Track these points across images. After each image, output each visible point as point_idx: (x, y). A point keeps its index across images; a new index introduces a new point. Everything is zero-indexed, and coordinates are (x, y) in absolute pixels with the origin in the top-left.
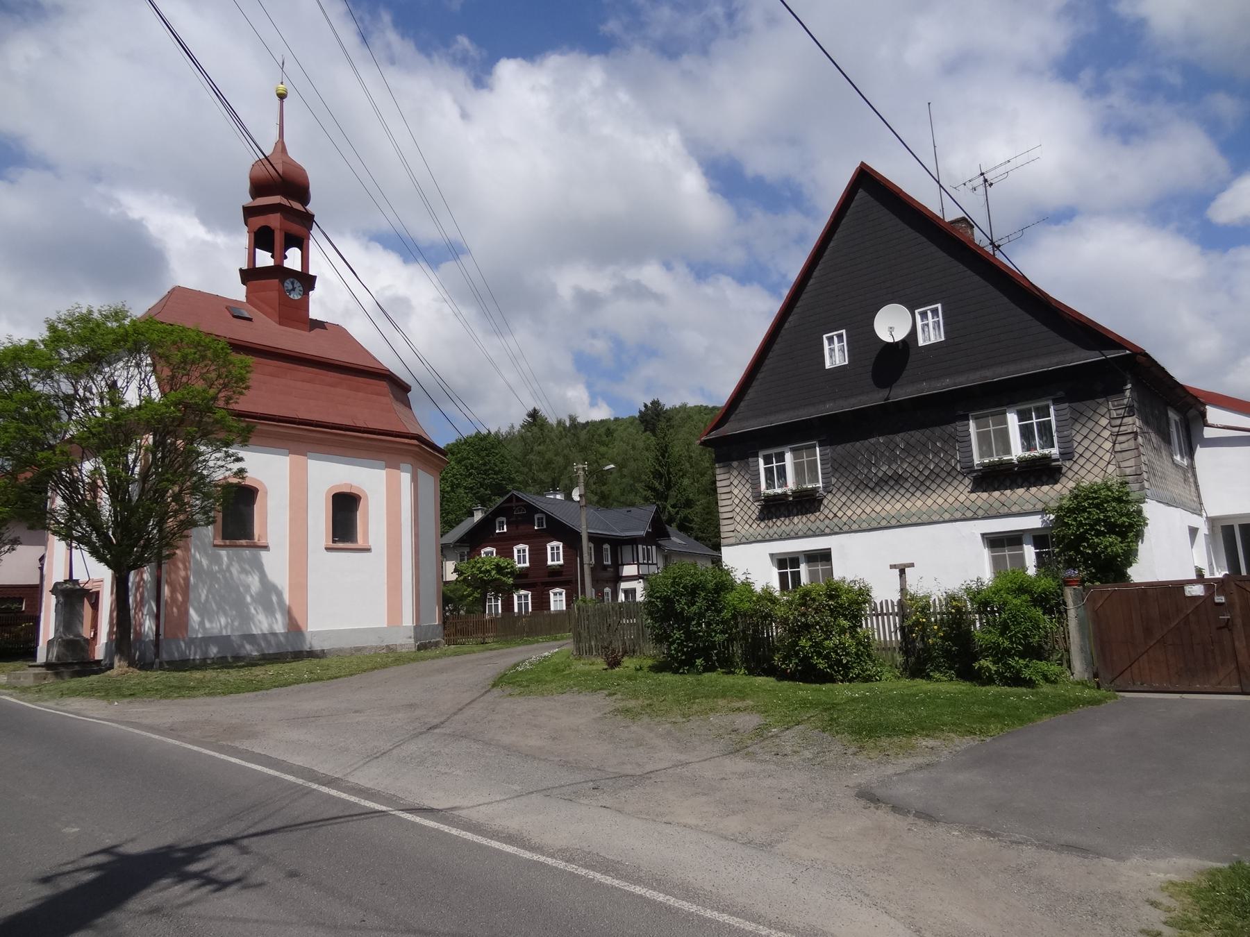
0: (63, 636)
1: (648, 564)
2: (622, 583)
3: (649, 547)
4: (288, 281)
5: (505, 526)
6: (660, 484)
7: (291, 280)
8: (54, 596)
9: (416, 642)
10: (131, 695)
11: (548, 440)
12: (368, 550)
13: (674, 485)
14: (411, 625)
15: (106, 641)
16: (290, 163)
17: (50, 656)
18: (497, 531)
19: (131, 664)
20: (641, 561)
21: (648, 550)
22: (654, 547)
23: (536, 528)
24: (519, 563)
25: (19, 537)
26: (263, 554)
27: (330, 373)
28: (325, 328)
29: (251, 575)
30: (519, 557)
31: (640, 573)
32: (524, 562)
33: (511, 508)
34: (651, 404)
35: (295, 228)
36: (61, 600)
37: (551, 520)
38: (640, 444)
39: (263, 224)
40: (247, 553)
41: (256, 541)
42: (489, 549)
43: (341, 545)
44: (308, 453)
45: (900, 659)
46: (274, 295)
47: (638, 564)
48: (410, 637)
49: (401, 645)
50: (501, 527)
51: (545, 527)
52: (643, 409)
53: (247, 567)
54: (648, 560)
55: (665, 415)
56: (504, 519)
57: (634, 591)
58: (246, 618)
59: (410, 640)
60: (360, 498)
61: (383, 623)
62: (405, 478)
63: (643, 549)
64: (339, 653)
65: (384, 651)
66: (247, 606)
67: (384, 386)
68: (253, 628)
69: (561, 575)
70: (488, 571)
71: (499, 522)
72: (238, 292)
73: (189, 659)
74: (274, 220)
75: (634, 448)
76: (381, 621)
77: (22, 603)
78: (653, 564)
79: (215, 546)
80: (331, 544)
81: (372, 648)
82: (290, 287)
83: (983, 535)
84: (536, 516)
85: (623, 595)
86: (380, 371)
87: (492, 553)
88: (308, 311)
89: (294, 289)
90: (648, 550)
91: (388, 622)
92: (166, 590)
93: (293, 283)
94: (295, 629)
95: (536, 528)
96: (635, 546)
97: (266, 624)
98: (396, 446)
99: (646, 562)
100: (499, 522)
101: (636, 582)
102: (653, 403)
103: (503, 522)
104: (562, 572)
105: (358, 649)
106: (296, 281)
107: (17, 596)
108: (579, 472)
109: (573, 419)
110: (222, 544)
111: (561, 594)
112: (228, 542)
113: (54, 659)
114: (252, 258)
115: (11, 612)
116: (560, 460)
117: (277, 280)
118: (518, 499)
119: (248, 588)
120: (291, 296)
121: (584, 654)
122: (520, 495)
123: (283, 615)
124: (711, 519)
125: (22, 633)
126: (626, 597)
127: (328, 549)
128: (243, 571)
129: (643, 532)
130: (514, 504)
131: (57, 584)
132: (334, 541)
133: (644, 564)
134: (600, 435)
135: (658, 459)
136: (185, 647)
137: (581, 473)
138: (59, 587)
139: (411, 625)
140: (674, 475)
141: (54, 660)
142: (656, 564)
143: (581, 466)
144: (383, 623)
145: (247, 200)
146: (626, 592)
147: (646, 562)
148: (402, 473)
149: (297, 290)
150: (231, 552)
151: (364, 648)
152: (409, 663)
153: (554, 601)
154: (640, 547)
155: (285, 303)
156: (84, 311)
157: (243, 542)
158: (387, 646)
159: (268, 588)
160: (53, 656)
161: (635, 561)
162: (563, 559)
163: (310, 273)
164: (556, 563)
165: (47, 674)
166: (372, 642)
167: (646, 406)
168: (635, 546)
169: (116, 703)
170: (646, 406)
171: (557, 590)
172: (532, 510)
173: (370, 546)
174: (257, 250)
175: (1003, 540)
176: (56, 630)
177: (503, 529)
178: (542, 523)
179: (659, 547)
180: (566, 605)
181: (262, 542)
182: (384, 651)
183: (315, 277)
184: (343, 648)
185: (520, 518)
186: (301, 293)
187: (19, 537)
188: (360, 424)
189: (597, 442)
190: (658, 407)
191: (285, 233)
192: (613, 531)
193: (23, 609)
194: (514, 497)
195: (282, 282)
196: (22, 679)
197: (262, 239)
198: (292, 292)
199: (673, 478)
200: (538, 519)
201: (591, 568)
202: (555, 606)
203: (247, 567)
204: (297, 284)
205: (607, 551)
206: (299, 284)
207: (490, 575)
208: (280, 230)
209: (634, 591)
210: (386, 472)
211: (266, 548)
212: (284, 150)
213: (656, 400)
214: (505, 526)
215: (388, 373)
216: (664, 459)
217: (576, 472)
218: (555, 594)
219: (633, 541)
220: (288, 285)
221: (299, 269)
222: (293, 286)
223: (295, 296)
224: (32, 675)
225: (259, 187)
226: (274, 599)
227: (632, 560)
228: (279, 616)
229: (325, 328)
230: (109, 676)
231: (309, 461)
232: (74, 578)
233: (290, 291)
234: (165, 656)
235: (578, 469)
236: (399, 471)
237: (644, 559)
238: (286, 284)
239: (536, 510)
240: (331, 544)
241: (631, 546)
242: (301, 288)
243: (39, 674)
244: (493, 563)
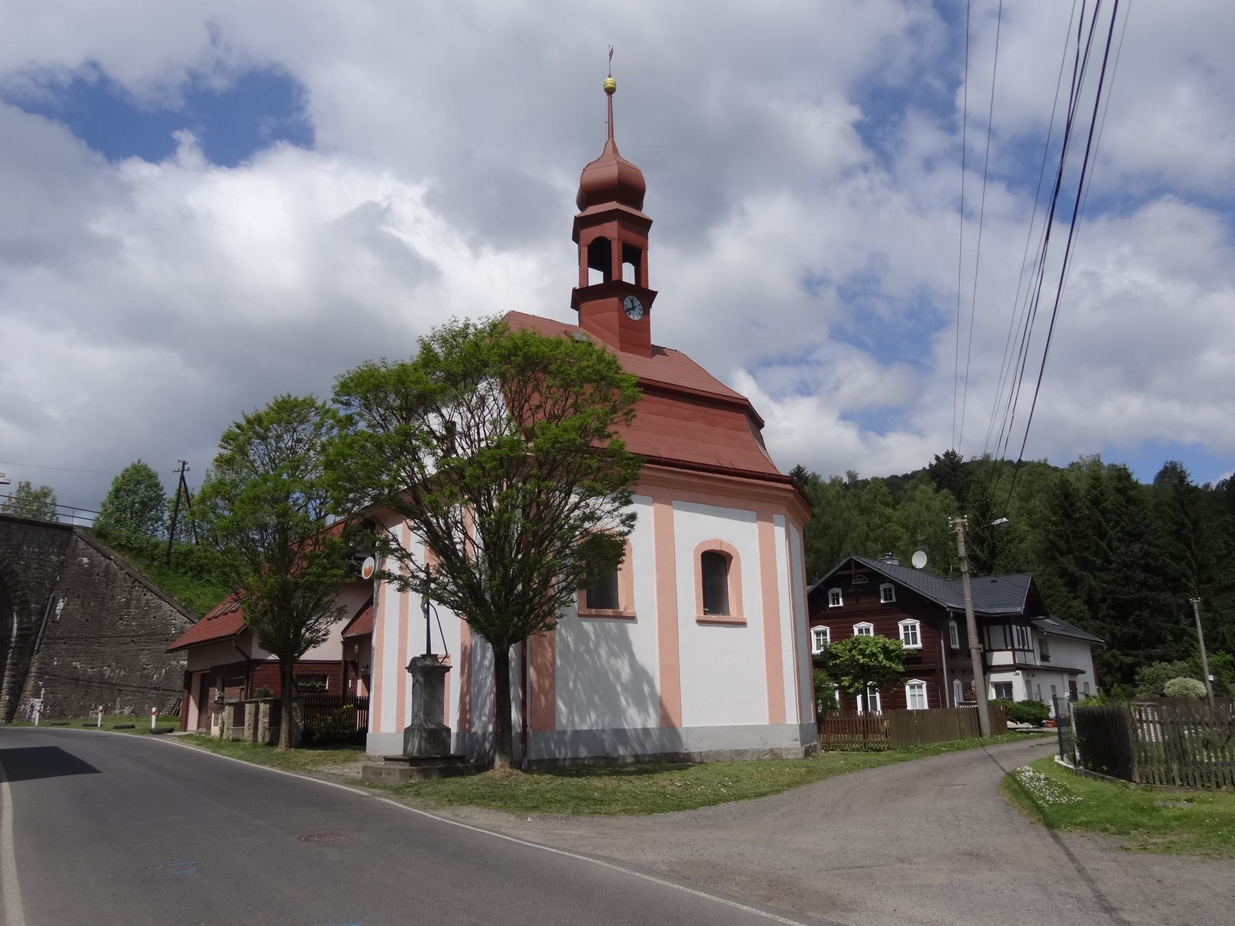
0: (424, 724)
1: (1024, 650)
2: (992, 675)
3: (1024, 628)
4: (627, 299)
5: (841, 600)
6: (982, 551)
7: (631, 297)
8: (411, 675)
9: (802, 744)
10: (534, 807)
11: (823, 501)
12: (743, 624)
13: (1001, 552)
14: (796, 723)
15: (456, 732)
16: (622, 165)
17: (410, 747)
18: (831, 606)
19: (516, 765)
20: (1016, 646)
21: (1022, 631)
22: (1029, 628)
23: (882, 601)
24: (908, 643)
25: (345, 606)
26: (630, 626)
27: (684, 404)
28: (664, 354)
29: (620, 657)
30: (906, 635)
31: (1017, 662)
32: (915, 642)
33: (850, 577)
34: (944, 455)
35: (632, 237)
36: (421, 679)
37: (902, 590)
38: (937, 505)
39: (598, 235)
40: (612, 625)
41: (622, 609)
42: (863, 625)
43: (714, 617)
44: (673, 501)
45: (595, 728)
46: (613, 317)
47: (1013, 650)
48: (796, 740)
49: (787, 749)
50: (836, 600)
51: (894, 600)
52: (934, 462)
53: (616, 648)
54: (1024, 645)
55: (961, 469)
56: (839, 591)
57: (1008, 686)
58: (618, 713)
59: (795, 743)
60: (730, 557)
61: (764, 720)
62: (779, 532)
63: (1017, 630)
64: (717, 756)
65: (767, 756)
66: (617, 695)
67: (742, 418)
68: (624, 723)
69: (920, 663)
70: (873, 655)
71: (833, 595)
72: (571, 318)
73: (558, 759)
74: (611, 230)
75: (928, 508)
76: (760, 717)
77: (326, 682)
78: (1029, 651)
79: (580, 616)
80: (702, 616)
81: (754, 752)
82: (630, 306)
83: (637, 623)
84: (882, 587)
85: (994, 690)
86: (737, 401)
87: (868, 631)
88: (649, 333)
89: (633, 308)
90: (1022, 631)
91: (771, 718)
92: (532, 673)
93: (632, 302)
94: (668, 724)
95: (882, 601)
96: (1007, 627)
97: (638, 719)
98: (761, 491)
99: (1021, 647)
100: (833, 595)
101: (1012, 673)
102: (947, 455)
103: (838, 594)
104: (921, 658)
105: (740, 753)
106: (635, 299)
107: (321, 673)
108: (957, 528)
109: (852, 476)
110: (588, 613)
111: (920, 687)
112: (593, 611)
113: (415, 751)
114: (584, 276)
115: (314, 692)
116: (839, 523)
117: (616, 298)
118: (859, 565)
119: (617, 675)
120: (631, 317)
121: (1157, 782)
122: (863, 560)
123: (655, 709)
124: (1054, 595)
125: (344, 716)
126: (998, 693)
127: (700, 622)
128: (612, 653)
129: (1020, 608)
130: (853, 571)
131: (414, 660)
132: (705, 613)
133: (1019, 650)
134: (884, 495)
135: (978, 520)
136: (555, 748)
137: (959, 529)
138: (419, 664)
139: (796, 723)
140: (1000, 539)
141: (415, 753)
142: (1033, 651)
143: (958, 520)
144: (764, 720)
145: (577, 212)
146: (998, 686)
147: (1021, 647)
148: (775, 527)
149: (637, 309)
150: (596, 624)
151: (746, 751)
152: (838, 774)
153: (911, 696)
154: (1014, 627)
155: (625, 323)
156: (461, 325)
157: (609, 612)
158: (771, 750)
159: (639, 673)
160: (413, 749)
161: (1008, 646)
162: (922, 642)
163: (650, 289)
164: (911, 646)
165: (412, 770)
166: (752, 743)
167: (937, 458)
168: (1007, 627)
169: (529, 820)
170: (937, 458)
171: (915, 681)
172: (877, 578)
173: (745, 619)
174: (589, 268)
175: (908, 627)
176: (414, 716)
177: (838, 603)
178: (891, 595)
179: (1035, 628)
180: (929, 702)
181: (628, 613)
182: (767, 756)
183: (655, 293)
184: (722, 751)
185: (860, 590)
186: (642, 312)
187: (345, 606)
188: (726, 464)
189: (882, 503)
190: (954, 459)
191: (623, 243)
192: (982, 608)
193: (327, 688)
194: (852, 561)
195: (622, 301)
196: (383, 776)
197: (597, 255)
198: (632, 311)
199: (997, 543)
200: (885, 590)
201: (981, 653)
202: (913, 703)
203: (616, 648)
204: (637, 303)
205: (954, 631)
206: (638, 302)
207: (877, 659)
208: (618, 240)
209: (1008, 686)
210: (758, 525)
211: (632, 619)
212: (615, 150)
213: (950, 451)
214: (841, 600)
215: (746, 403)
216: (984, 519)
217: (953, 529)
218: (912, 687)
219: (1005, 620)
220: (628, 303)
221: (633, 282)
222: (633, 305)
223: (635, 316)
224: (397, 772)
225: (588, 196)
226: (646, 689)
227: (1005, 645)
228: (651, 711)
229: (664, 354)
230: (491, 778)
231: (675, 512)
232: (432, 653)
233: (629, 310)
234: (533, 756)
235: (955, 525)
236: (772, 524)
237: (1019, 644)
238: (625, 303)
239: (884, 579)
240: (702, 616)
241: (1001, 627)
242: (641, 307)
243: (405, 770)
244: (879, 645)
